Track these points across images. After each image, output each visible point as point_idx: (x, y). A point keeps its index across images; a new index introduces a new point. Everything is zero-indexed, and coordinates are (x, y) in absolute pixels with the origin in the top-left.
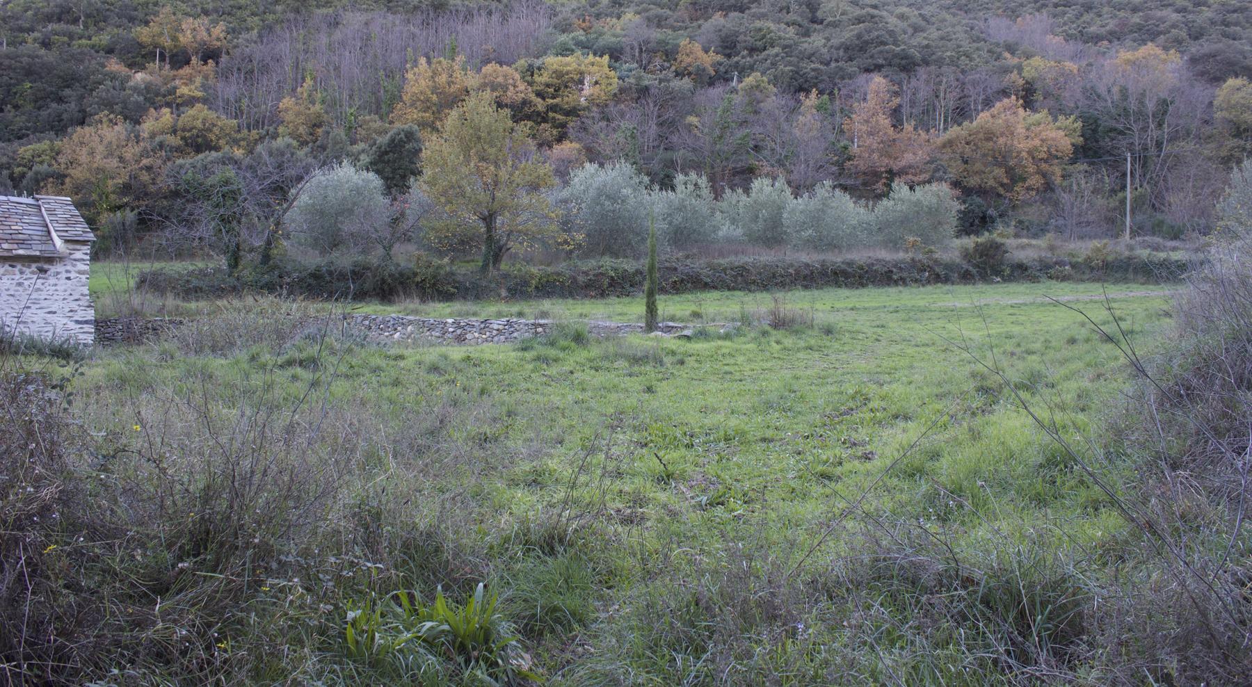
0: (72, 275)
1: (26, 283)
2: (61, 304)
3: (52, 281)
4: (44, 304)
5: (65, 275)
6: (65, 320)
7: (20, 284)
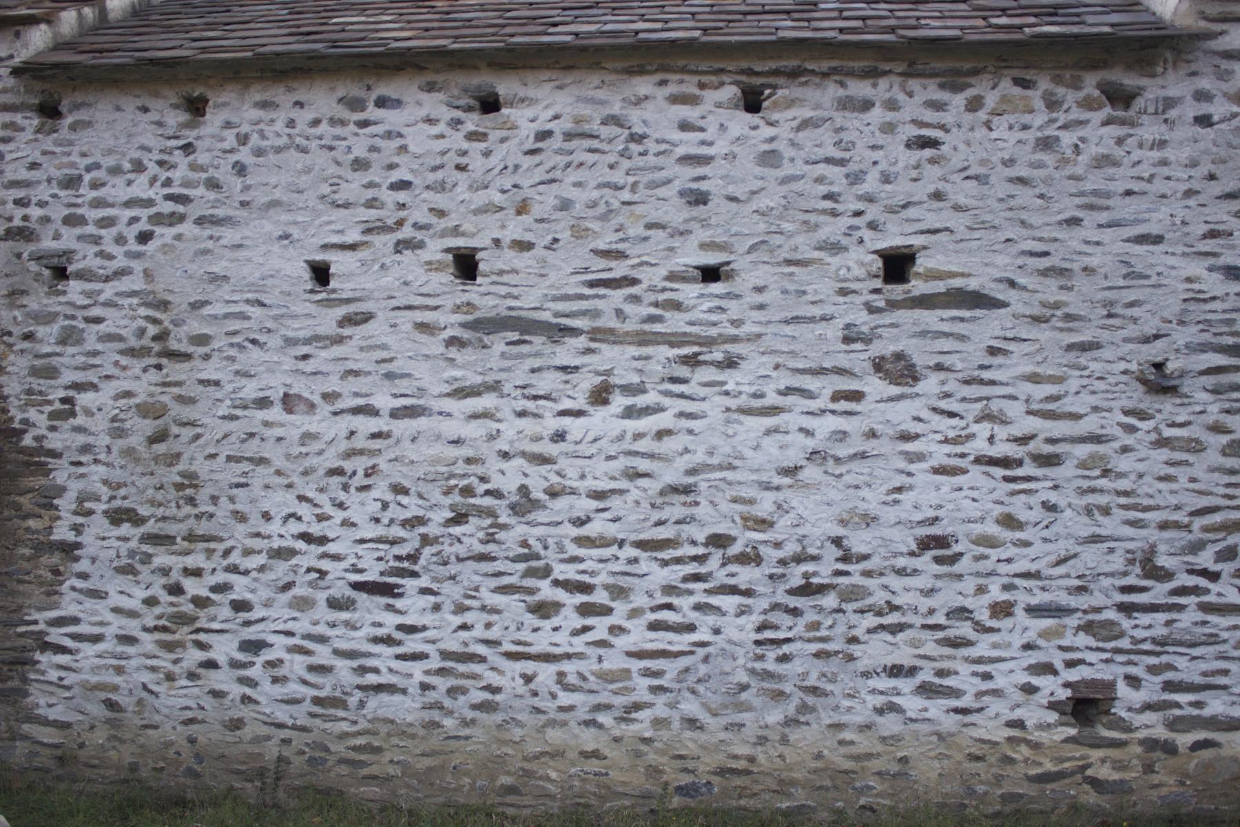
0: (1218, 109)
1: (1068, 138)
2: (1177, 208)
3: (1150, 130)
4: (1125, 209)
5: (1191, 110)
6: (1197, 268)
7: (1046, 144)
